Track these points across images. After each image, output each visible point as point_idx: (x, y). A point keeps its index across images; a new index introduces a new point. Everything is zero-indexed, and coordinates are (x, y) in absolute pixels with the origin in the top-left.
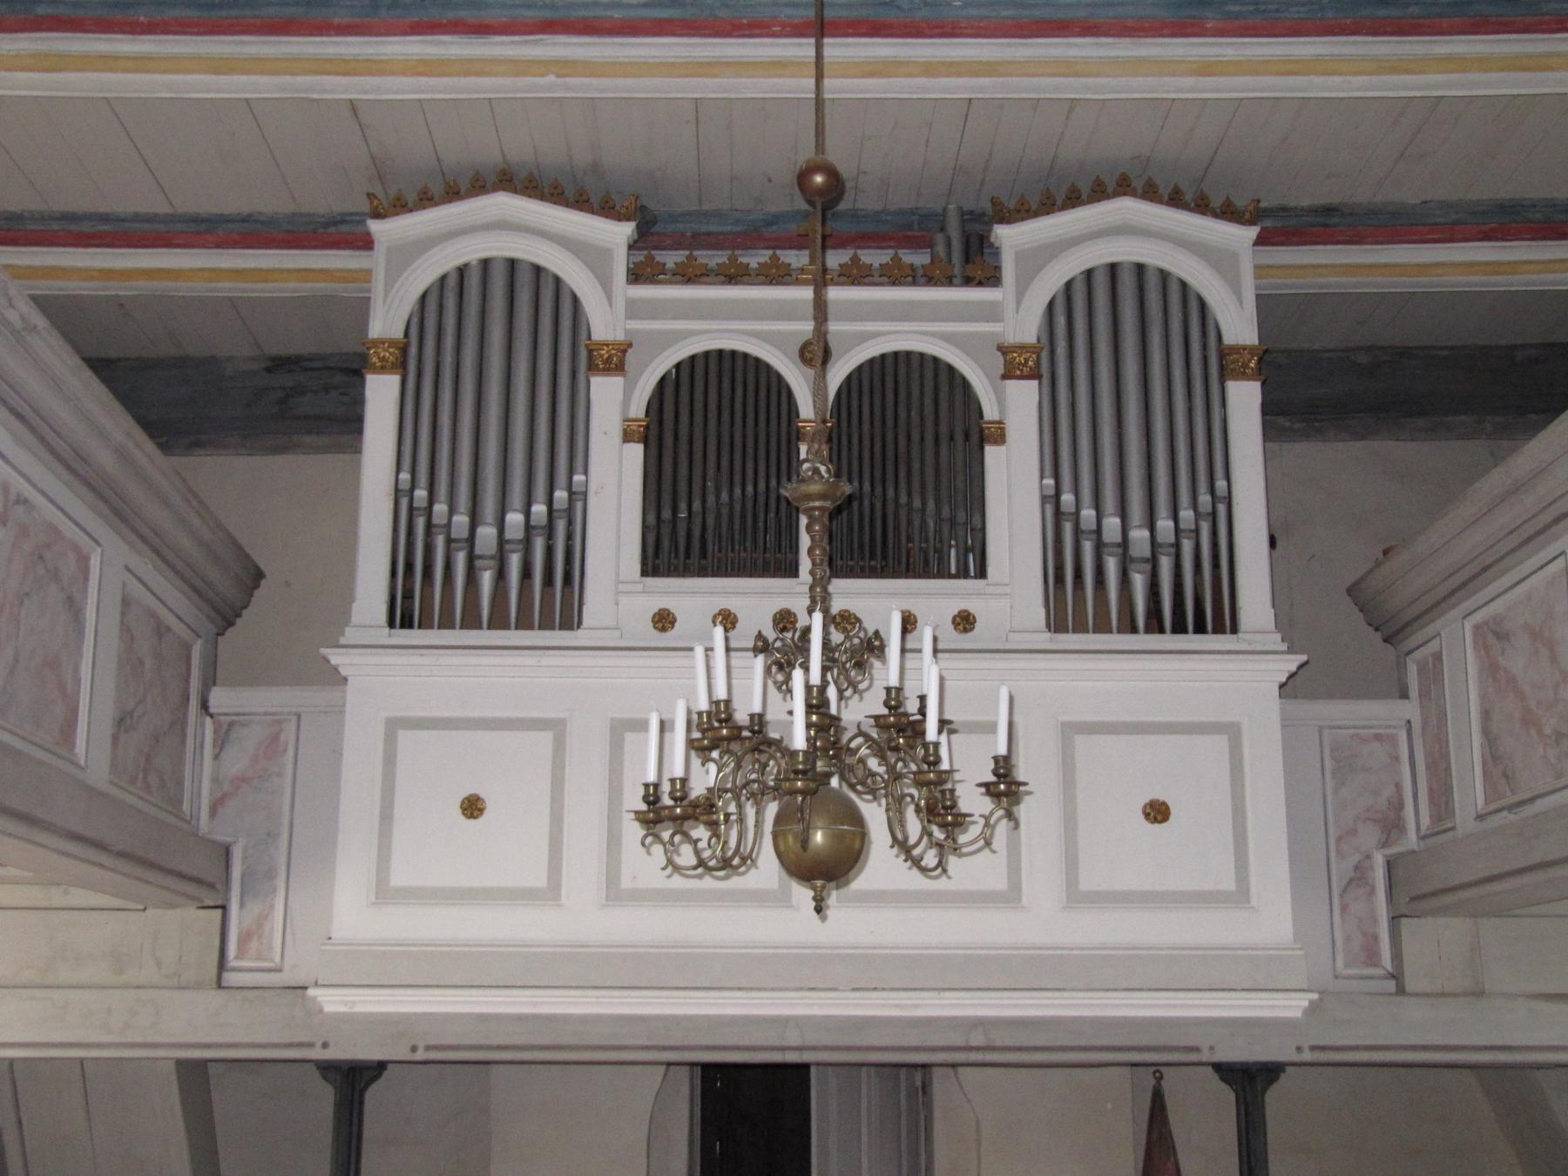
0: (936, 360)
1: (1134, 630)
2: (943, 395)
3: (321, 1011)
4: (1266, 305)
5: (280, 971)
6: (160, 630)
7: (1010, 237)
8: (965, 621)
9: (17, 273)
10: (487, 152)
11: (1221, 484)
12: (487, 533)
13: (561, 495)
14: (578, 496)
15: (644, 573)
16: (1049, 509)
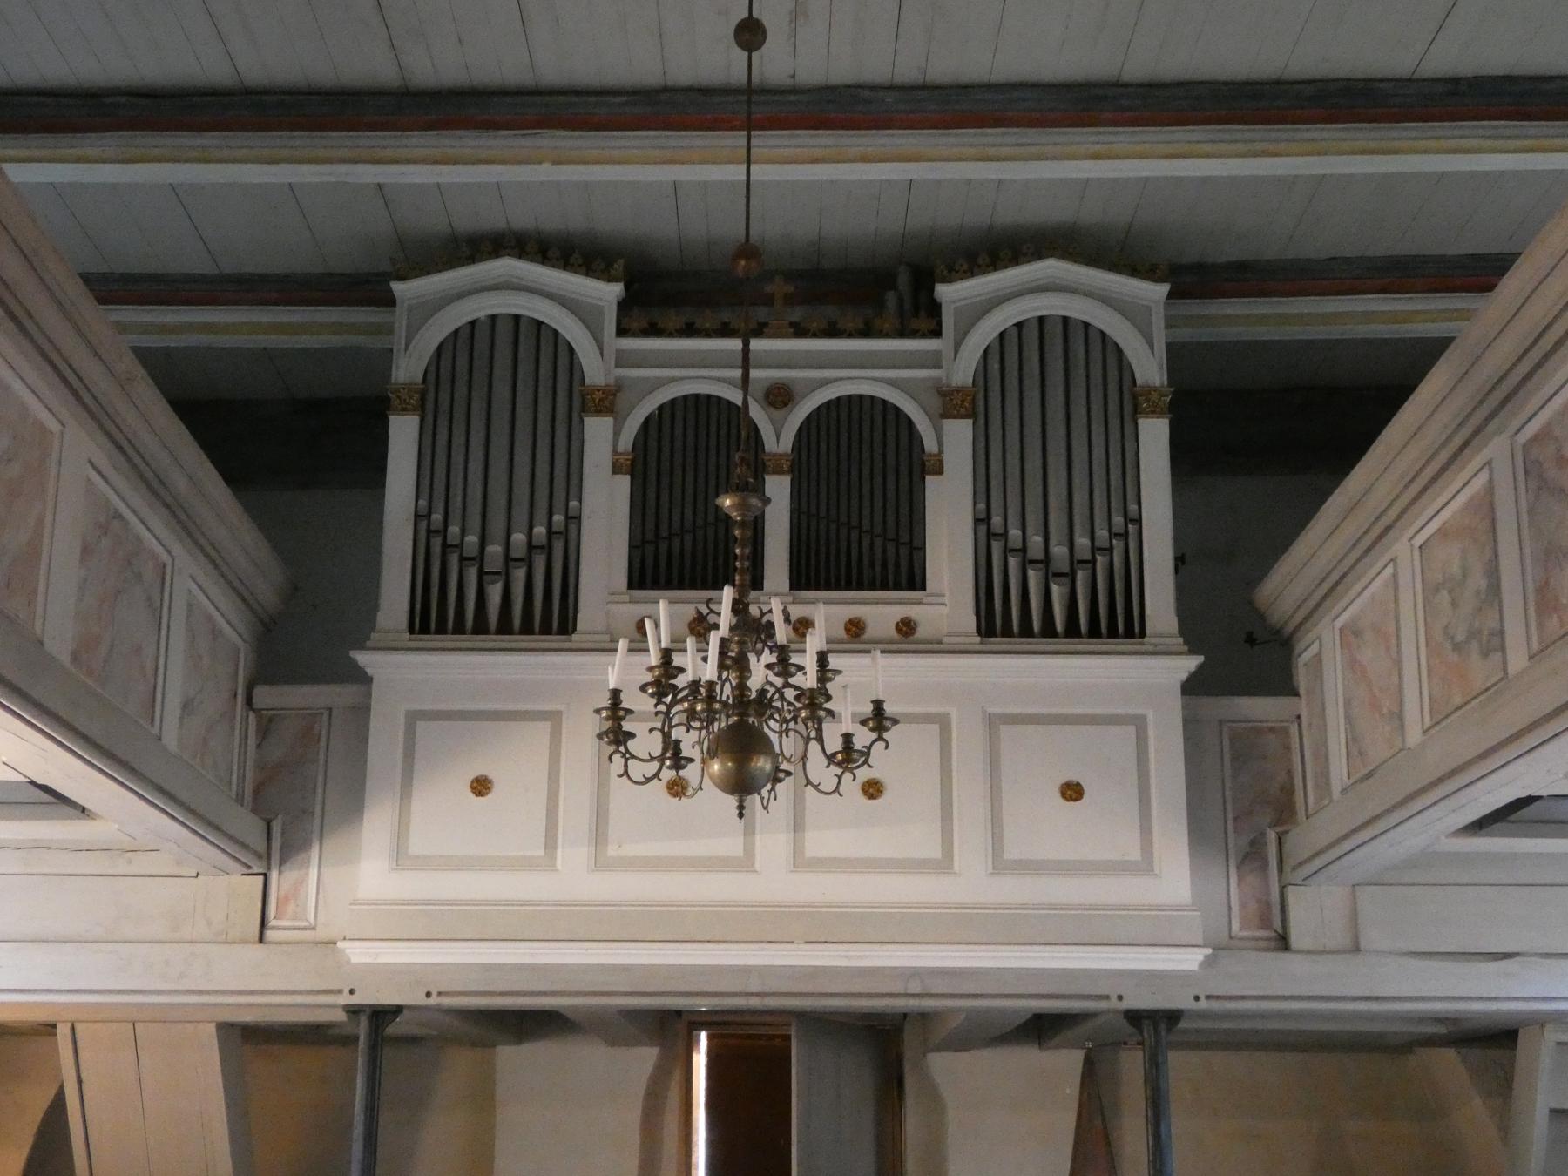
0: (884, 402)
1: (1054, 634)
2: (891, 433)
3: (348, 962)
4: (1175, 353)
5: (314, 929)
6: (215, 633)
7: (949, 293)
8: (906, 628)
9: (122, 328)
10: (492, 219)
11: (1133, 507)
12: (494, 549)
13: (558, 518)
14: (574, 519)
15: (631, 586)
16: (983, 528)
